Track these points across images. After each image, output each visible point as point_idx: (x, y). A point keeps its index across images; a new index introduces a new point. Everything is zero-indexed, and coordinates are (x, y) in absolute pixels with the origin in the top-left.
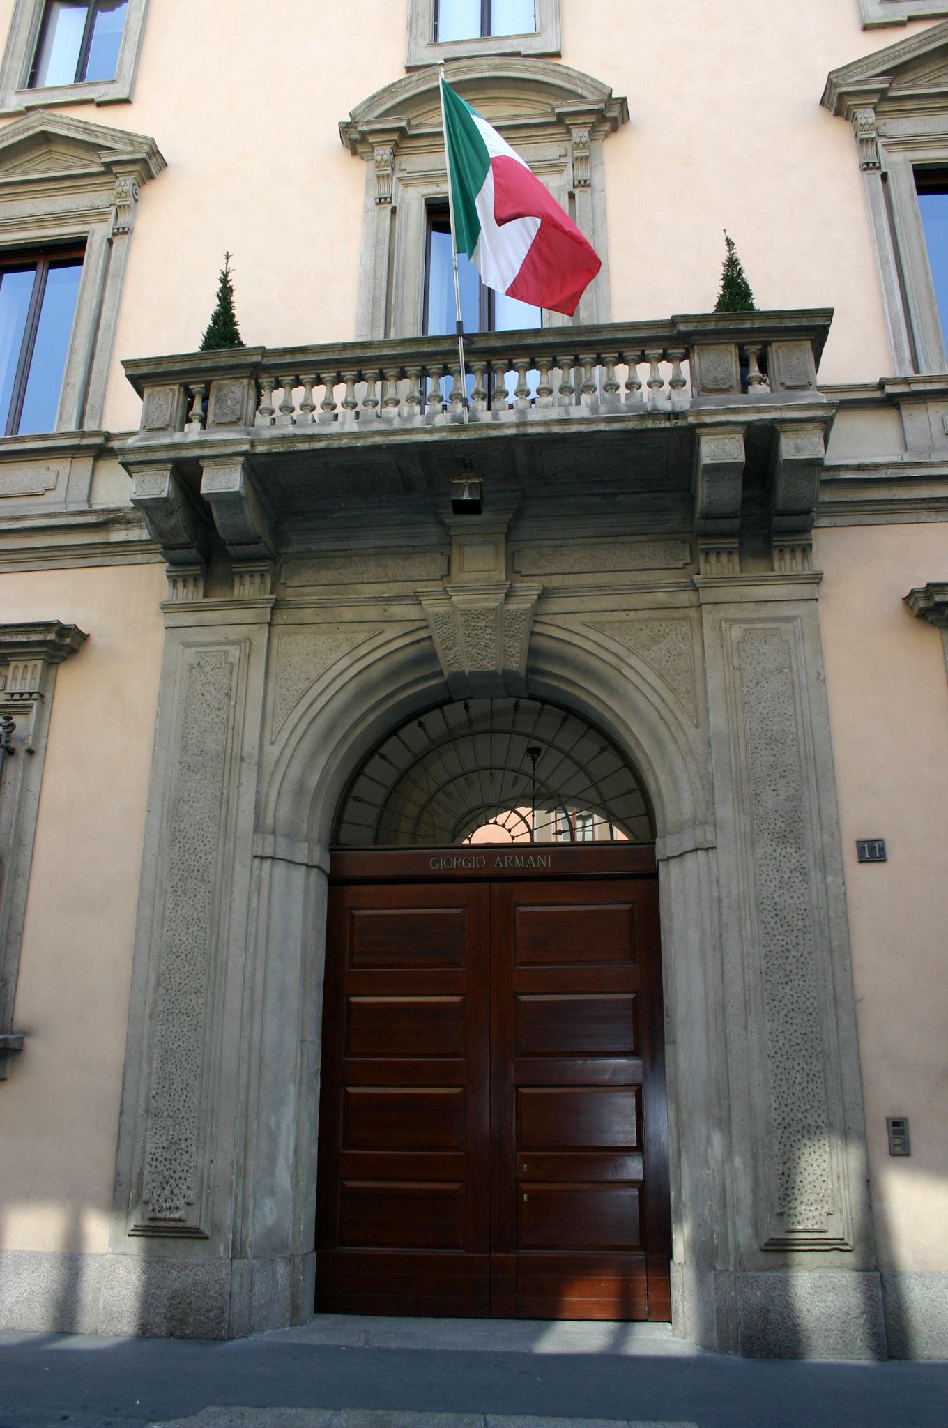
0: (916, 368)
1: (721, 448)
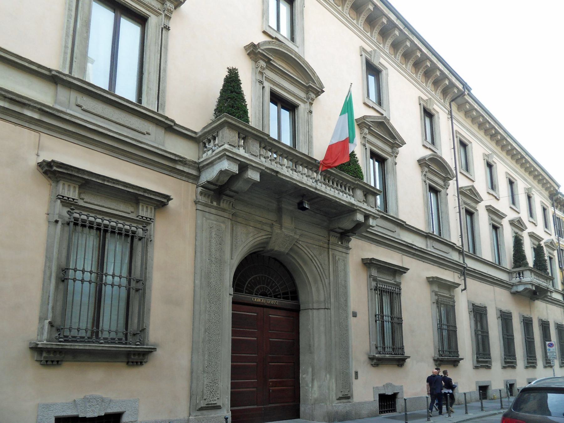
0: (70, 72)
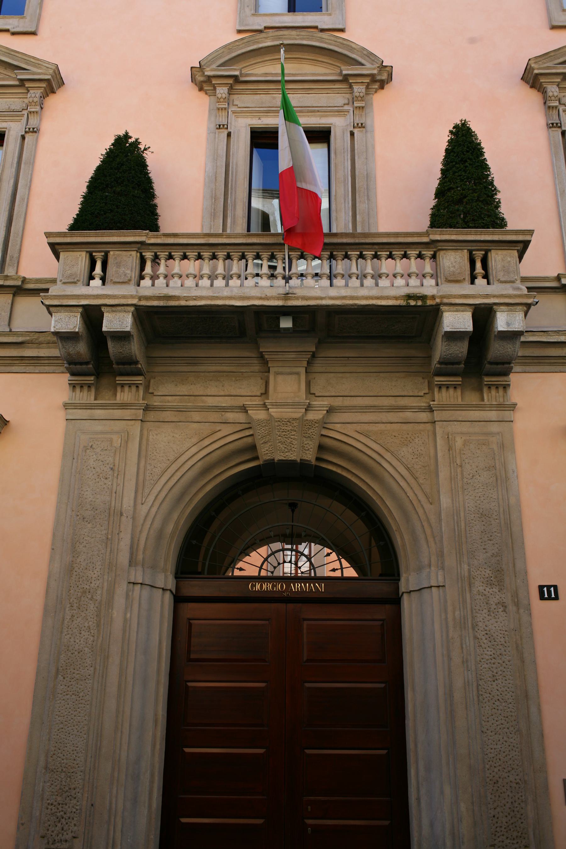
1: (458, 321)
